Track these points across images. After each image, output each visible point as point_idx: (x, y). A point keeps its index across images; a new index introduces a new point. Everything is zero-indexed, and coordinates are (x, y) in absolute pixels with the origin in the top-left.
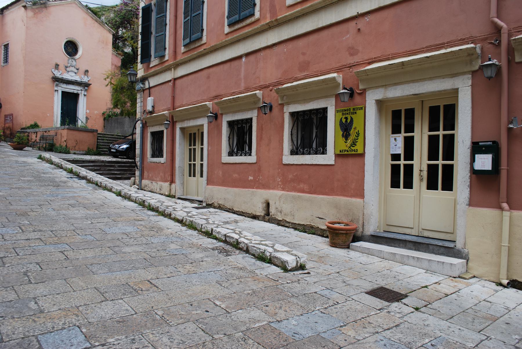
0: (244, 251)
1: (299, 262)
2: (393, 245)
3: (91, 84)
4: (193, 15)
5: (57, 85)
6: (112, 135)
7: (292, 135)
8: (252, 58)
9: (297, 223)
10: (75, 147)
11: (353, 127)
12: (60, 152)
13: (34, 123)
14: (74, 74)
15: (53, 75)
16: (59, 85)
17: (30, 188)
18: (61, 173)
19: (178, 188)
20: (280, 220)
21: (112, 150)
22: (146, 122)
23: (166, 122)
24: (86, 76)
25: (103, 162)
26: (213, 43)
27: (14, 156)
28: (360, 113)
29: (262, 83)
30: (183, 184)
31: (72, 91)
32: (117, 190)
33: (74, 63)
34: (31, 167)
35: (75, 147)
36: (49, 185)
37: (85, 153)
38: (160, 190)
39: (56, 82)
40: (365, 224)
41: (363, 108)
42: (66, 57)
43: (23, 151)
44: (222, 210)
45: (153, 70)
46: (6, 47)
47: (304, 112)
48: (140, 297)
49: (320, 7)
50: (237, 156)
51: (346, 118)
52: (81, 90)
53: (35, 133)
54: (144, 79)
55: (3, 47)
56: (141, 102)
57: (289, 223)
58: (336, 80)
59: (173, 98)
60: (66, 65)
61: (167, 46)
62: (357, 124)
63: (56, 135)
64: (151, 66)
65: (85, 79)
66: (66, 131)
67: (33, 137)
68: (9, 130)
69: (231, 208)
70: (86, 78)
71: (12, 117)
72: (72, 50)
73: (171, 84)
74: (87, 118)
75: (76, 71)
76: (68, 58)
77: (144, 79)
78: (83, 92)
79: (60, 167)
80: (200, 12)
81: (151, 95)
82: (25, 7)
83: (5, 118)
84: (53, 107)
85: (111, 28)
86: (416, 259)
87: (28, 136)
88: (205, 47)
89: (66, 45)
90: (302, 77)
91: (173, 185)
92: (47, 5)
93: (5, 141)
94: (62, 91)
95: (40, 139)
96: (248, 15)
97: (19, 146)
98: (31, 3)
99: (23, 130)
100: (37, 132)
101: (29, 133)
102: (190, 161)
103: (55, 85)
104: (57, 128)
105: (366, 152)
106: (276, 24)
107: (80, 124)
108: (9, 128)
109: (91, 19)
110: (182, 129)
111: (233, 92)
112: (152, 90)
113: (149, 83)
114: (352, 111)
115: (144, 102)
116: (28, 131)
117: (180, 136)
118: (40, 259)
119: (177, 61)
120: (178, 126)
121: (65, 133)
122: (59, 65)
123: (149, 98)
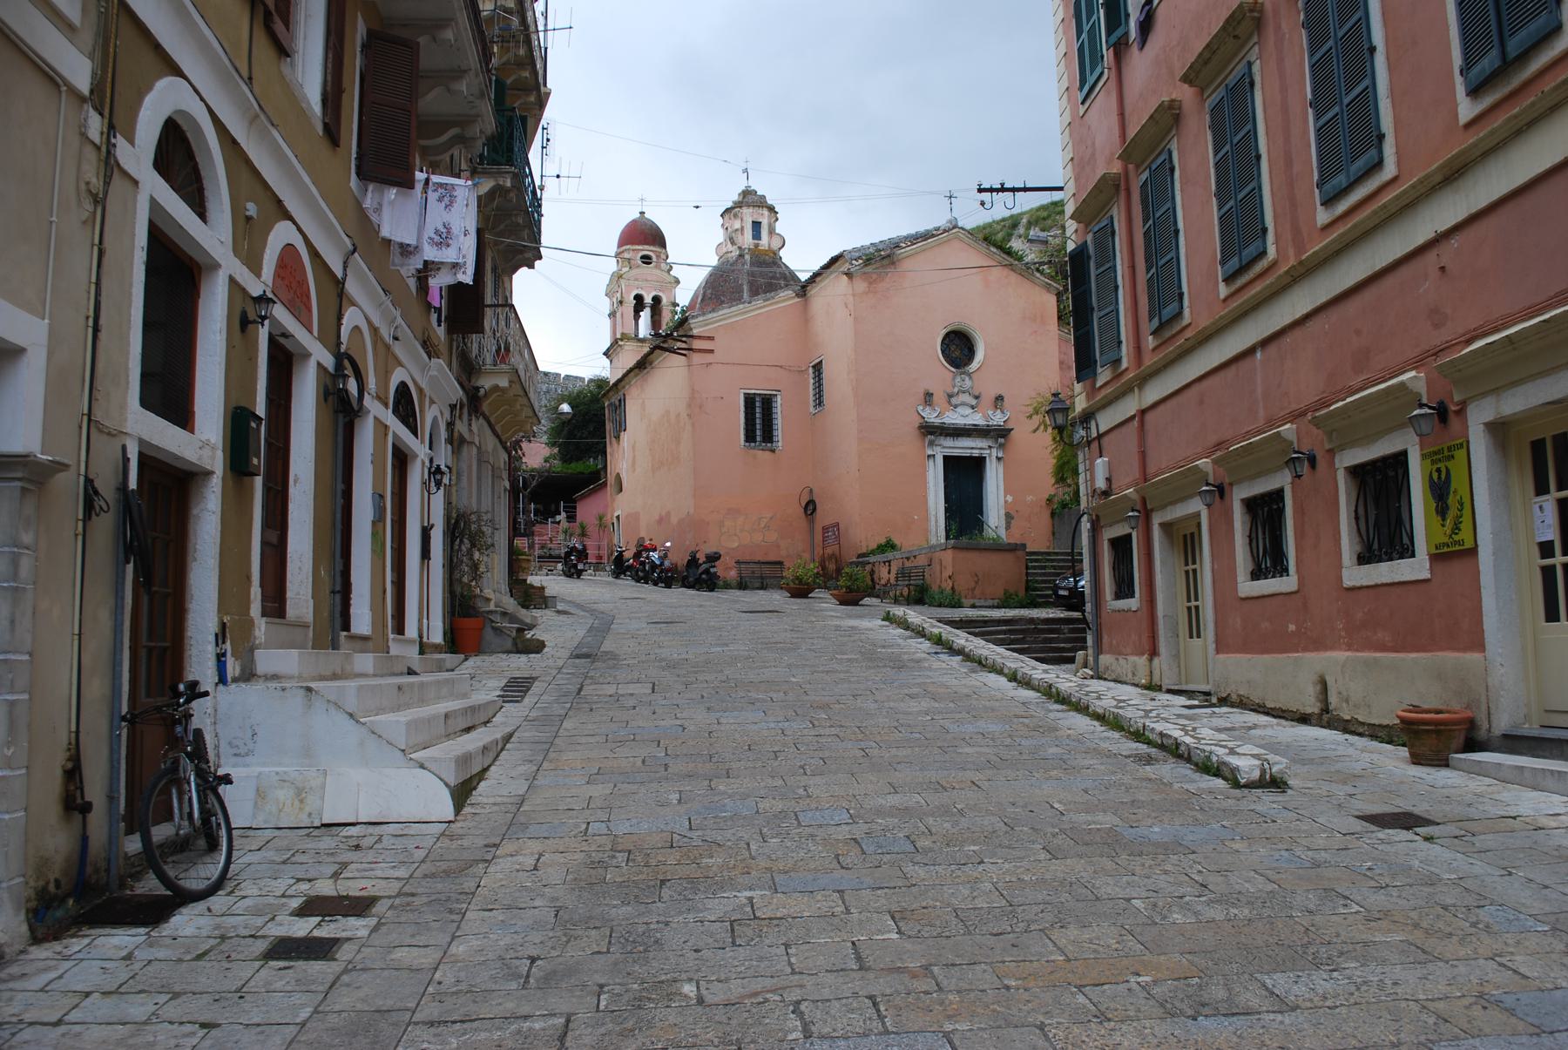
0: (1186, 759)
1: (1268, 771)
2: (1541, 753)
4: (1160, 264)
5: (931, 444)
7: (1357, 518)
8: (1272, 349)
9: (1376, 722)
10: (973, 589)
11: (1452, 489)
14: (968, 411)
17: (847, 672)
18: (919, 646)
19: (1165, 667)
20: (1347, 721)
21: (1062, 592)
22: (1097, 516)
23: (1130, 514)
25: (1032, 621)
26: (1204, 322)
27: (837, 617)
28: (1460, 454)
29: (1294, 406)
30: (1177, 656)
31: (967, 453)
32: (1010, 668)
34: (863, 637)
35: (973, 589)
36: (885, 666)
38: (1134, 674)
40: (1492, 712)
41: (1465, 445)
42: (947, 372)
43: (858, 608)
44: (1245, 709)
45: (1104, 393)
46: (818, 368)
47: (1373, 463)
48: (945, 794)
49: (1372, 225)
50: (1266, 578)
51: (1439, 470)
54: (1087, 417)
55: (811, 370)
56: (1086, 470)
57: (1363, 724)
58: (1407, 388)
59: (1143, 455)
61: (1123, 338)
62: (1459, 483)
64: (1098, 385)
65: (998, 419)
66: (950, 552)
67: (883, 574)
69: (1261, 702)
70: (998, 416)
72: (961, 350)
73: (1136, 423)
75: (974, 402)
77: (1087, 417)
78: (994, 451)
79: (921, 633)
80: (1173, 254)
81: (1104, 454)
82: (849, 274)
83: (824, 533)
85: (1051, 278)
86: (1556, 775)
87: (872, 572)
88: (1189, 334)
90: (1360, 385)
91: (1156, 661)
92: (895, 259)
93: (826, 588)
96: (1254, 255)
97: (851, 598)
98: (861, 261)
99: (861, 560)
100: (889, 562)
101: (874, 564)
102: (1189, 600)
105: (1479, 543)
106: (1303, 271)
107: (989, 533)
110: (1167, 527)
111: (1243, 431)
112: (1105, 441)
113: (1097, 425)
114: (1446, 453)
115: (1091, 470)
116: (872, 559)
117: (1161, 543)
118: (827, 754)
119: (1142, 368)
120: (1157, 520)
121: (948, 556)
123: (1099, 461)
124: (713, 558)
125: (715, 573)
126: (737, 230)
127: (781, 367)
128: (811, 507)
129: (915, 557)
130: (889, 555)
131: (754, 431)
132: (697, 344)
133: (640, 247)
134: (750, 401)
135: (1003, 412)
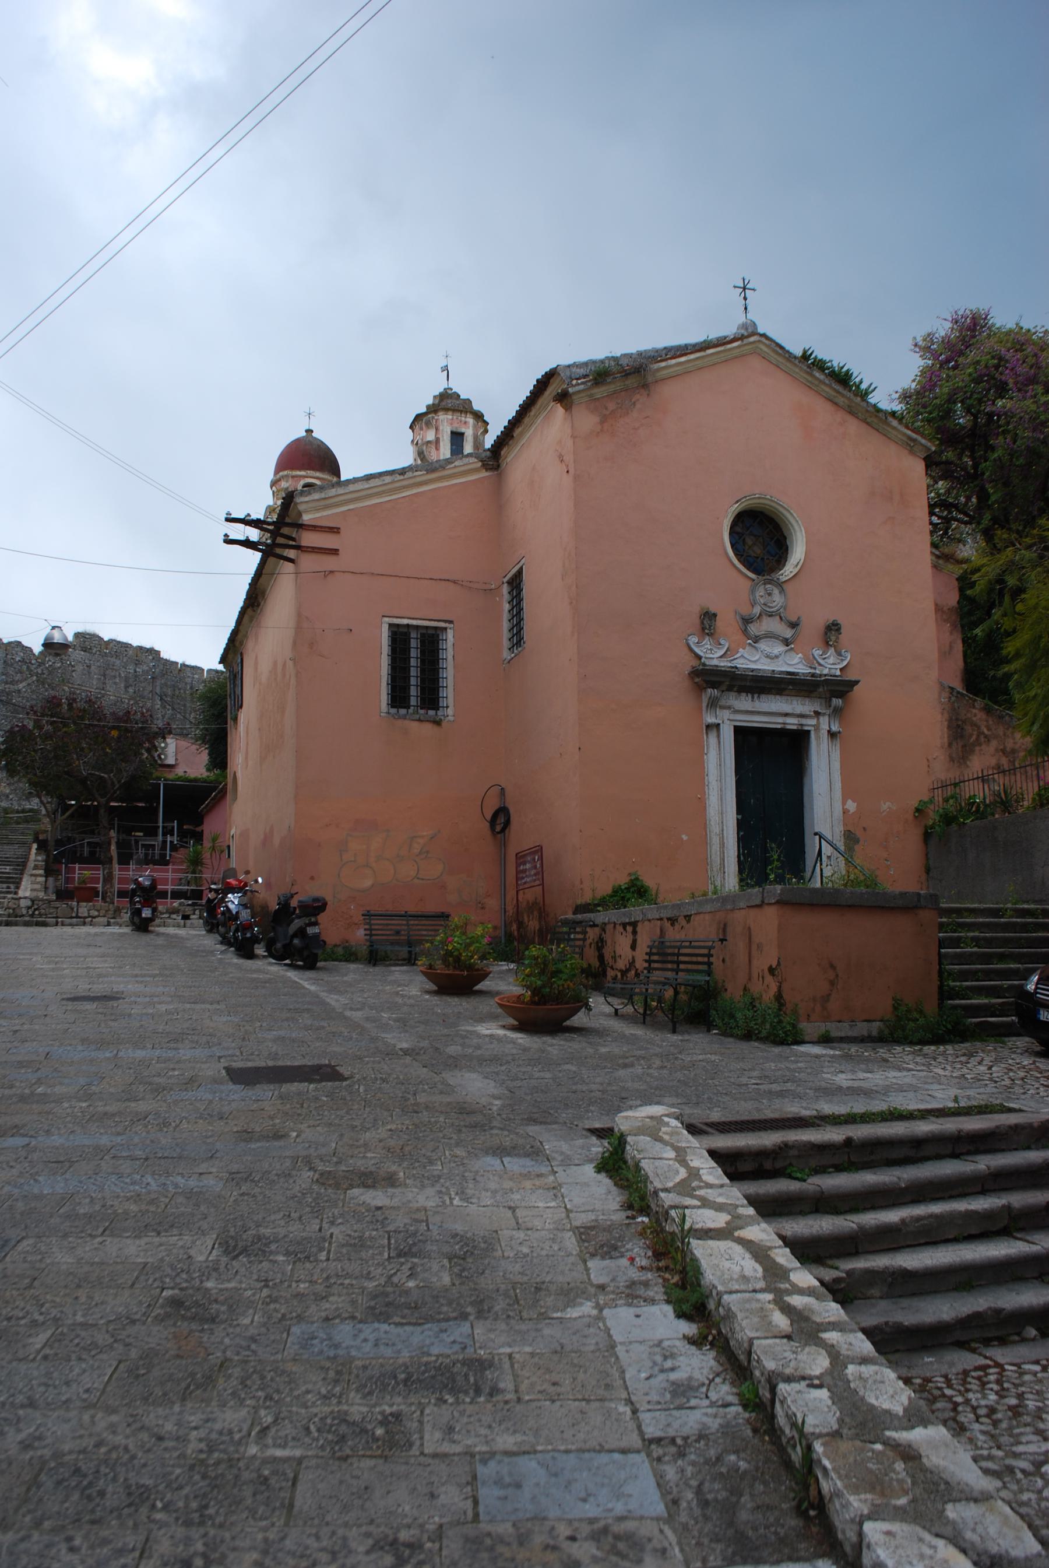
3: (857, 682)
5: (713, 704)
6: (995, 913)
10: (826, 998)
12: (748, 1036)
13: (627, 880)
14: (779, 648)
15: (695, 663)
16: (722, 702)
24: (832, 650)
33: (777, 599)
35: (826, 998)
37: (881, 1031)
39: (709, 690)
46: (516, 583)
52: (817, 714)
53: (629, 929)
55: (505, 589)
60: (745, 611)
63: (722, 940)
65: (830, 665)
66: (771, 913)
67: (621, 945)
68: (536, 913)
70: (831, 660)
71: (541, 858)
74: (850, 837)
75: (788, 633)
76: (749, 583)
84: (701, 803)
89: (738, 529)
92: (650, 379)
94: (735, 727)
95: (649, 962)
99: (579, 917)
100: (634, 924)
103: (704, 705)
104: (725, 899)
108: (532, 907)
109: (829, 406)
116: (601, 917)
122: (715, 615)
124: (315, 908)
125: (317, 936)
126: (429, 442)
127: (454, 582)
128: (501, 819)
129: (688, 918)
130: (635, 911)
131: (406, 688)
132: (308, 539)
133: (303, 473)
134: (399, 637)
135: (839, 654)
